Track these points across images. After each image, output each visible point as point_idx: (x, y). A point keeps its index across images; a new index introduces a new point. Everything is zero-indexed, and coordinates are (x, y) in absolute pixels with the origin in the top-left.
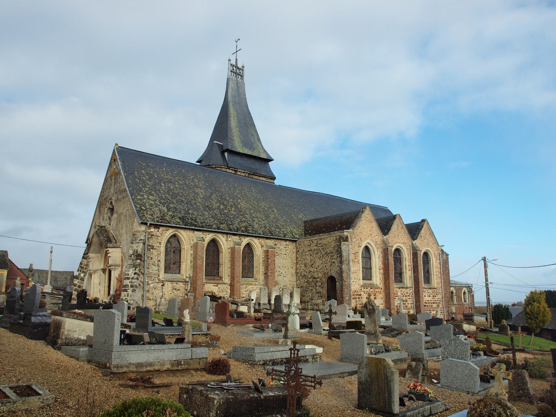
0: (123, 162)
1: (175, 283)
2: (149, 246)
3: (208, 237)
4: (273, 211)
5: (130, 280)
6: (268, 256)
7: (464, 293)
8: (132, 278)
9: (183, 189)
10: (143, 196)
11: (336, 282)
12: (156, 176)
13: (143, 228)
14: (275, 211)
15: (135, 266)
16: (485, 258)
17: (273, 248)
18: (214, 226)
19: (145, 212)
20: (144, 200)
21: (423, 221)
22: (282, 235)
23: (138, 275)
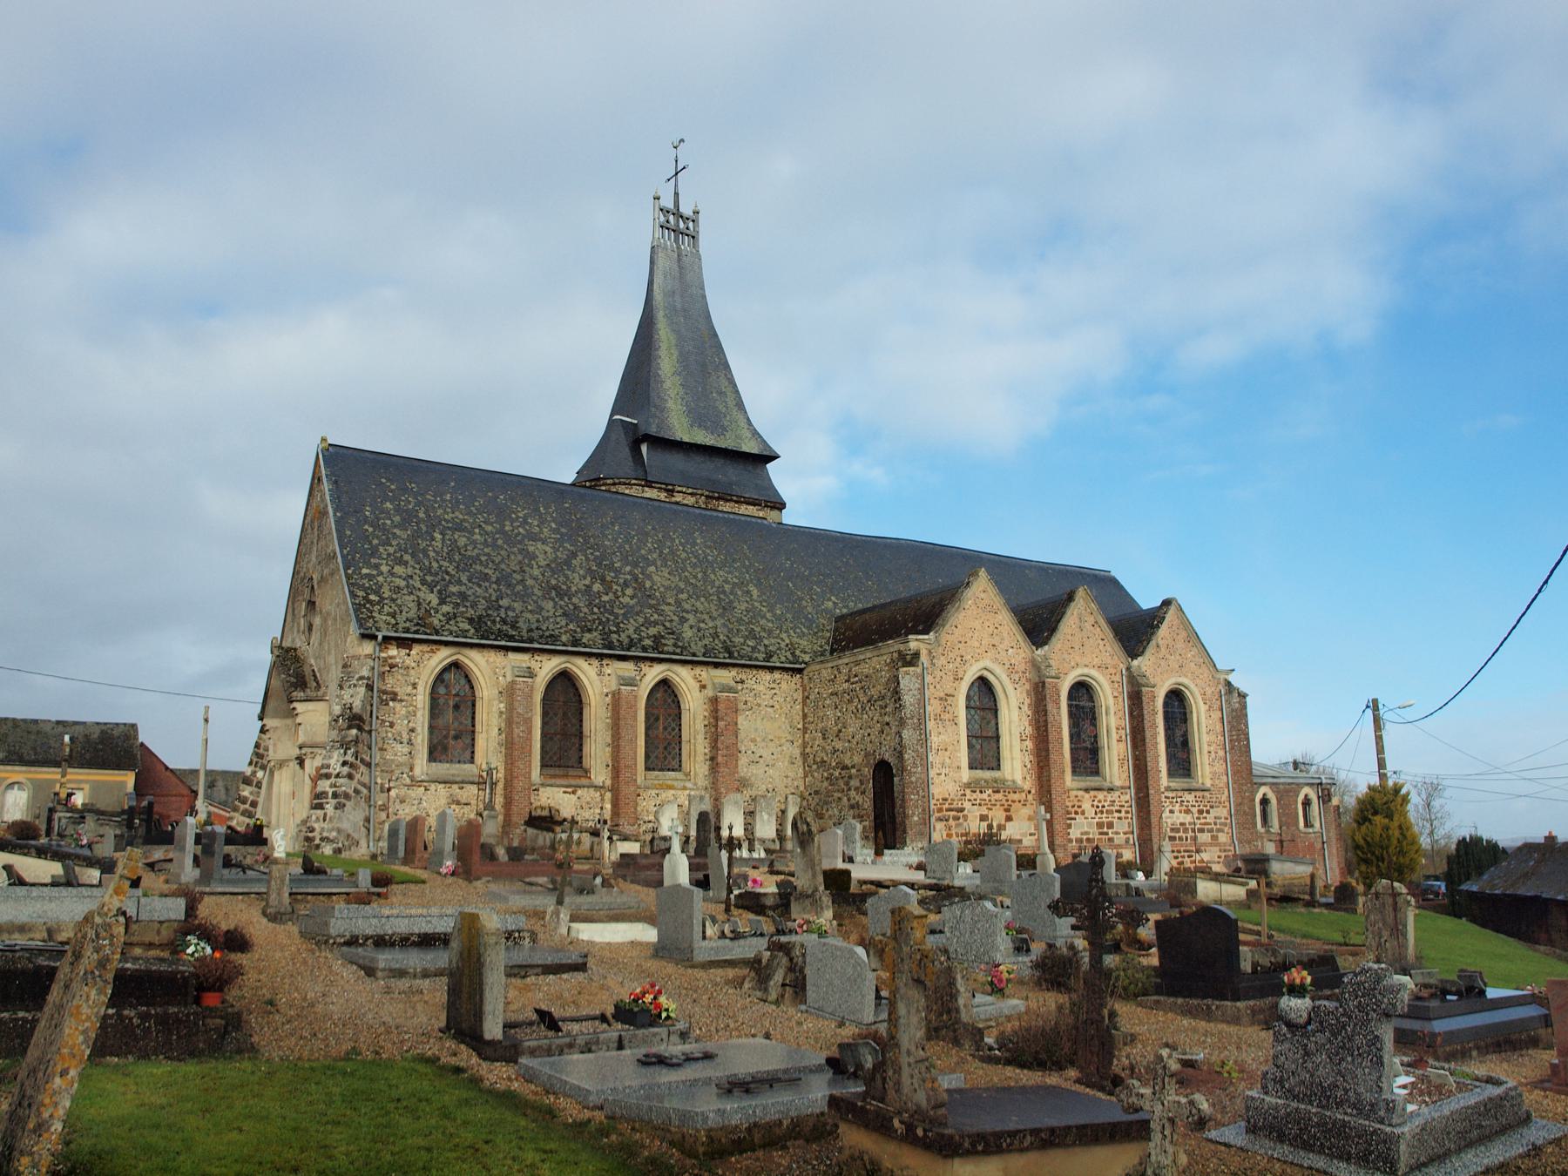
0: (336, 482)
1: (455, 786)
2: (385, 692)
3: (547, 667)
4: (748, 592)
5: (333, 780)
6: (716, 711)
7: (1307, 803)
8: (337, 776)
9: (494, 546)
10: (377, 566)
11: (892, 776)
12: (422, 515)
13: (368, 648)
14: (755, 593)
15: (345, 745)
16: (1375, 702)
17: (730, 690)
18: (564, 638)
19: (377, 608)
20: (380, 579)
21: (1167, 603)
22: (761, 656)
23: (352, 766)
